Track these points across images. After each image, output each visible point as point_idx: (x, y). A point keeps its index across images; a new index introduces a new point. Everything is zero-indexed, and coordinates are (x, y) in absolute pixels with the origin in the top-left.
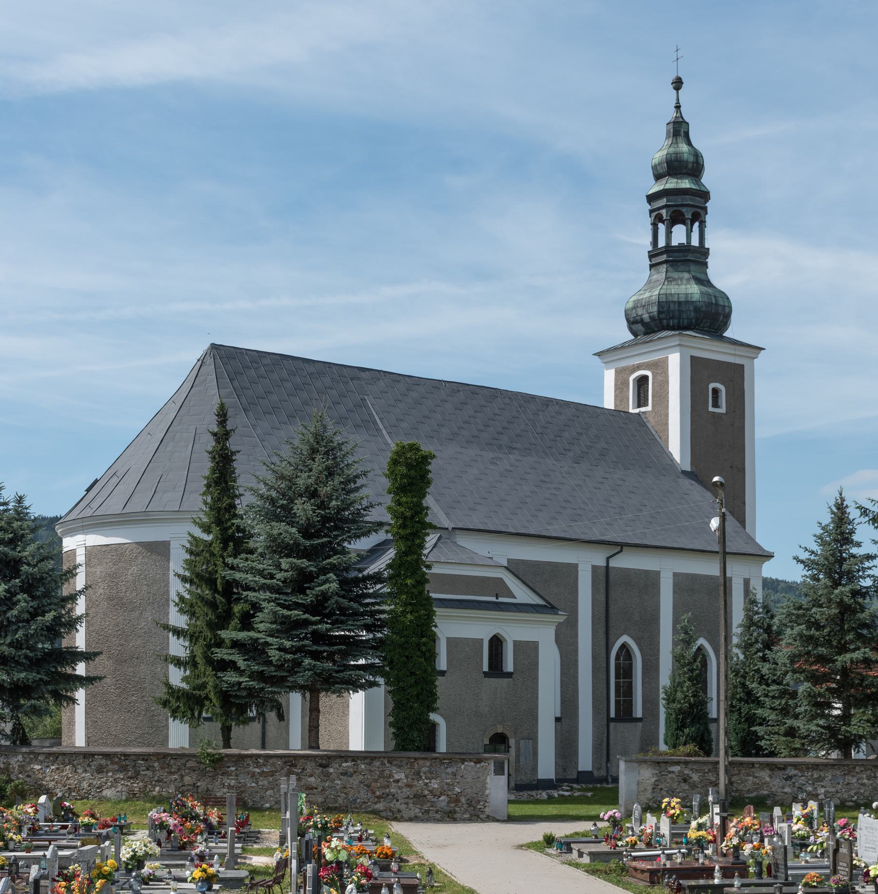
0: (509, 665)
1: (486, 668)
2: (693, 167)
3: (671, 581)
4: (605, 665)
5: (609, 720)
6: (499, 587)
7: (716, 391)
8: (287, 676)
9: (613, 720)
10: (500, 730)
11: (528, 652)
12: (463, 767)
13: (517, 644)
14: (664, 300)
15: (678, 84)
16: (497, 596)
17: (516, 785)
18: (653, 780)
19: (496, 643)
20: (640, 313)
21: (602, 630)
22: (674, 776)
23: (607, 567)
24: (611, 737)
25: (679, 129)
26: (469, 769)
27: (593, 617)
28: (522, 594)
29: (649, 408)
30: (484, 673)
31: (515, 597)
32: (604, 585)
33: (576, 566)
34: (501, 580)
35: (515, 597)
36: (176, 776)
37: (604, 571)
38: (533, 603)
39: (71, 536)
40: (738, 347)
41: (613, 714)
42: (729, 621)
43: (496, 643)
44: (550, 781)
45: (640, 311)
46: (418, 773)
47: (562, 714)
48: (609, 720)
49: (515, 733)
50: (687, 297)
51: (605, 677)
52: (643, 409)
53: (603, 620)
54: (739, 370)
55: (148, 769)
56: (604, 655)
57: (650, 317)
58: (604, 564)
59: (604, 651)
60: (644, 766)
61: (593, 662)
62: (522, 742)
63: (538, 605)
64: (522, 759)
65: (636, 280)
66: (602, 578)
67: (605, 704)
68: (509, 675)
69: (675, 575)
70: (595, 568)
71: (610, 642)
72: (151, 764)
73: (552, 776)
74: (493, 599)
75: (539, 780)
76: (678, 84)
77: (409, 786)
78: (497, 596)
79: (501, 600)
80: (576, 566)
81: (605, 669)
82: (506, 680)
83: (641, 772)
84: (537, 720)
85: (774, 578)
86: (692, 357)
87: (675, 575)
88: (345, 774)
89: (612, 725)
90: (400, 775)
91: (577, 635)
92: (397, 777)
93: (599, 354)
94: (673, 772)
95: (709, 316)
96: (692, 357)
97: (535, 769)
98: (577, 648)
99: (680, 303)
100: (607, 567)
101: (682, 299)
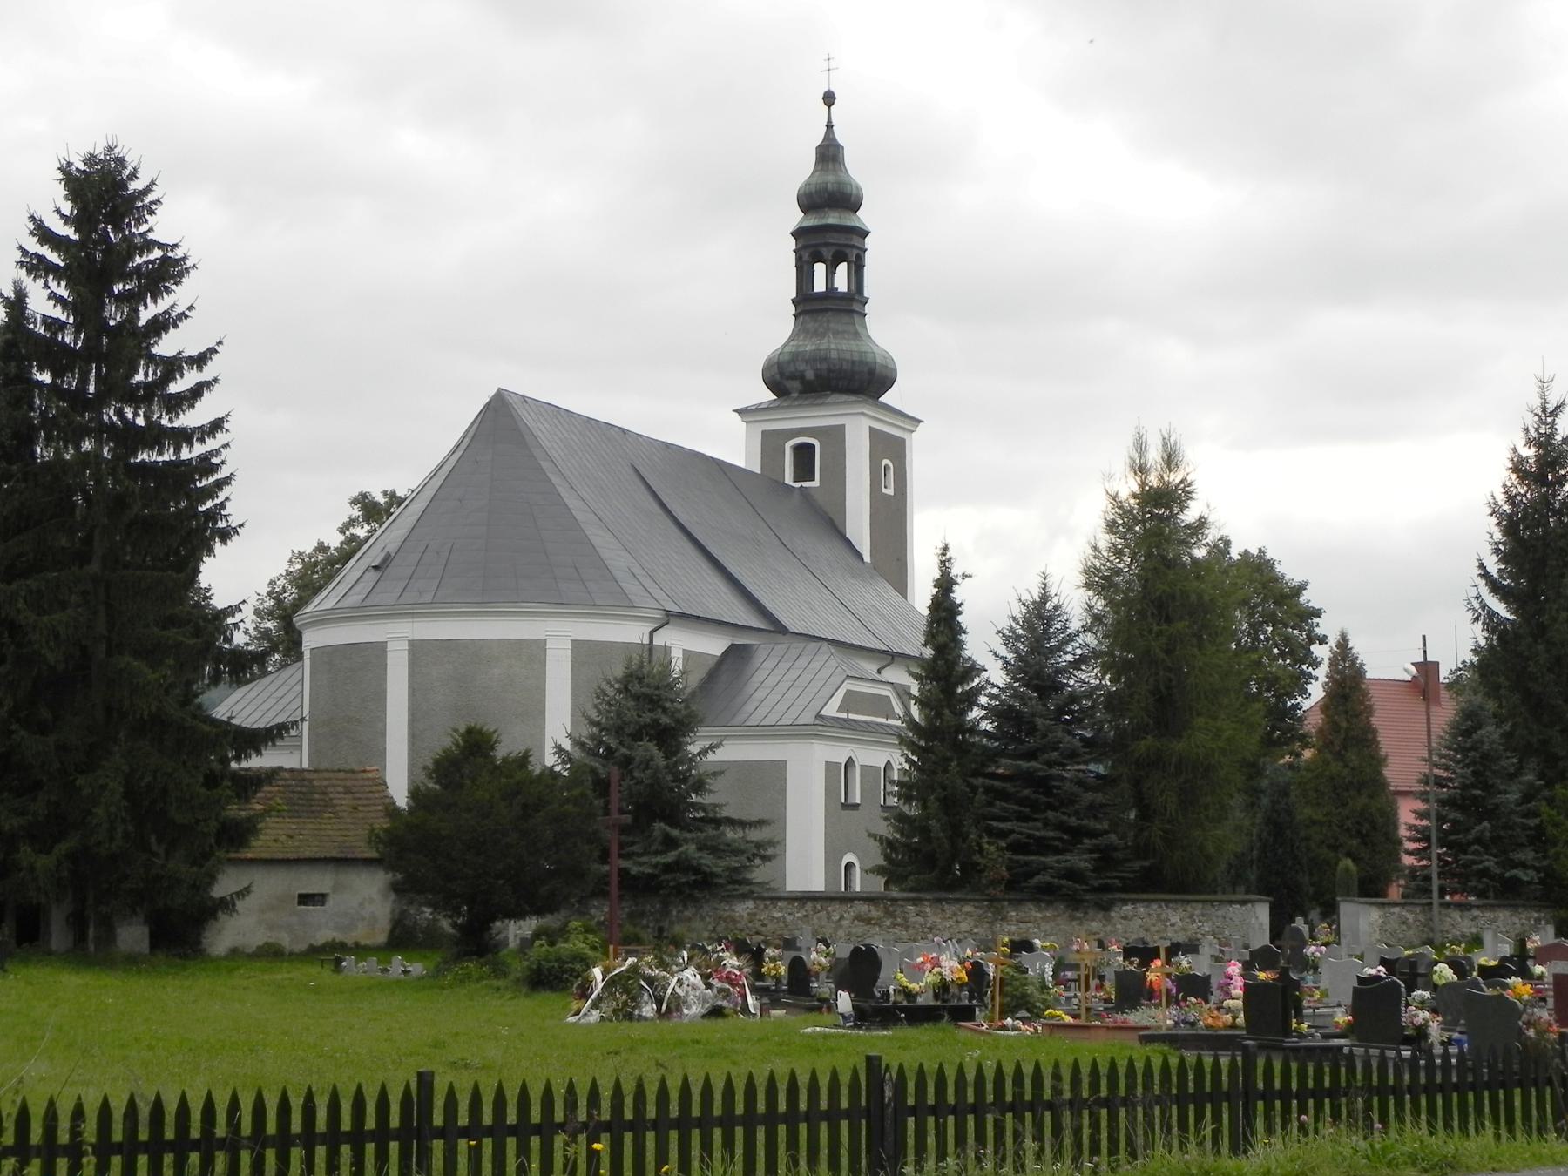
2: (849, 201)
15: (829, 99)
25: (829, 153)
29: (816, 483)
39: (1369, 711)
45: (802, 367)
46: (1191, 916)
54: (901, 444)
58: (646, 641)
65: (774, 327)
69: (577, 646)
73: (817, 884)
76: (829, 99)
77: (1183, 929)
85: (1375, 721)
87: (577, 646)
88: (1125, 918)
90: (1175, 919)
92: (1173, 920)
95: (867, 381)
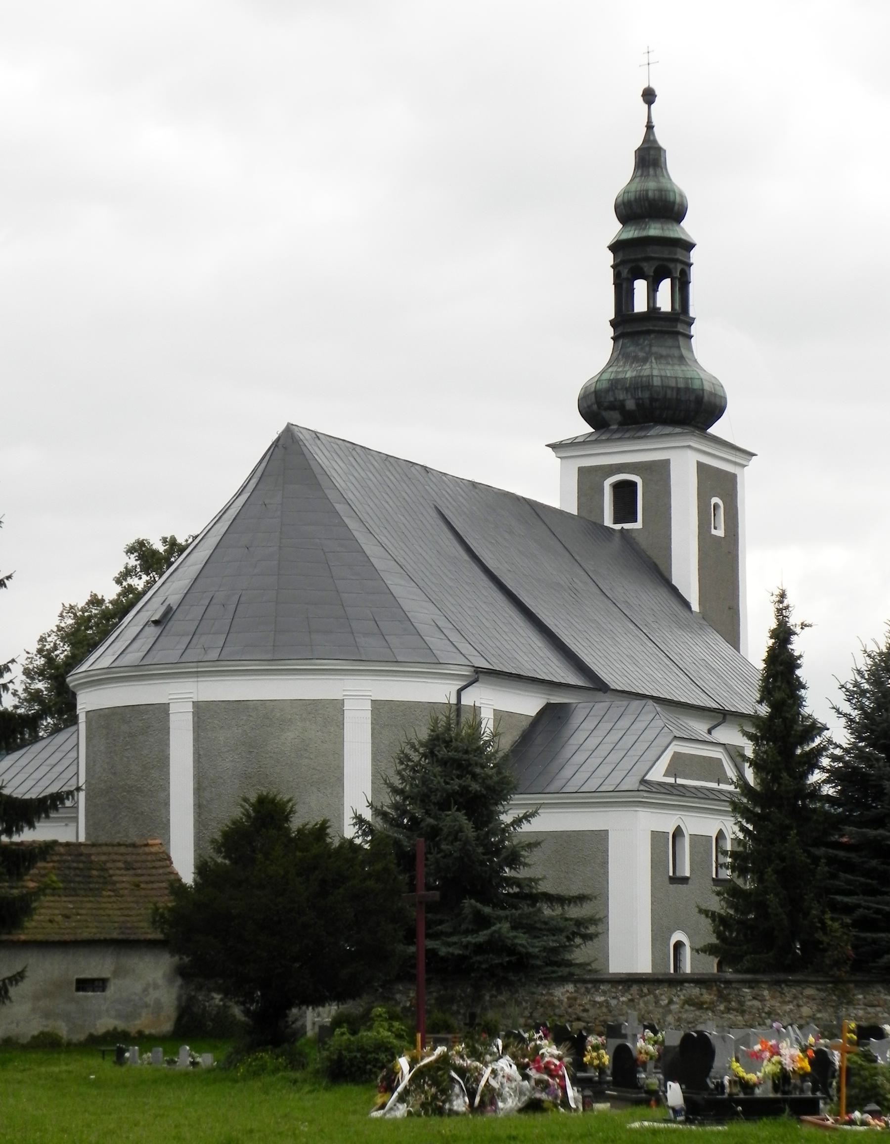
2: (671, 210)
7: (716, 506)
14: (659, 383)
15: (649, 96)
20: (621, 397)
25: (649, 157)
29: (638, 525)
36: (791, 1007)
40: (738, 453)
45: (621, 396)
50: (687, 383)
52: (627, 526)
54: (731, 480)
55: (754, 998)
57: (637, 405)
58: (453, 701)
65: (592, 353)
69: (377, 706)
72: (760, 993)
76: (649, 96)
86: (698, 462)
87: (377, 706)
93: (553, 446)
95: (695, 410)
96: (698, 462)
99: (678, 390)
101: (681, 385)
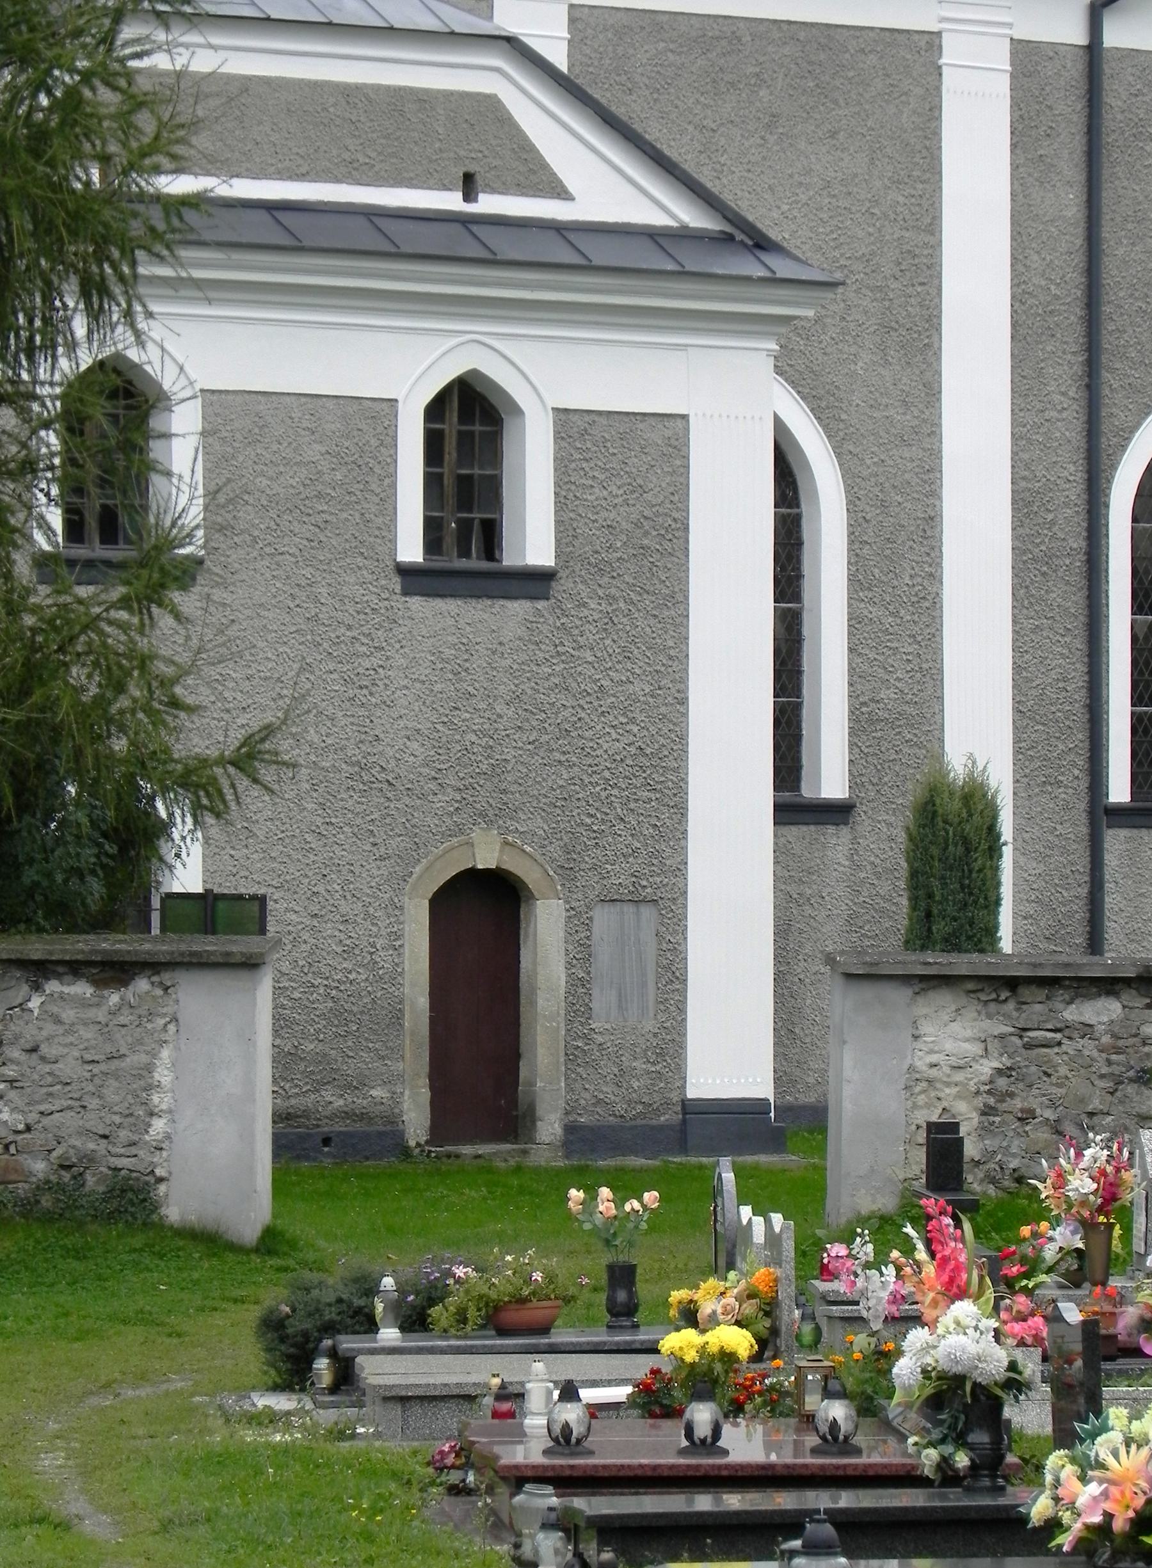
0: (533, 540)
1: (411, 548)
3: (999, 89)
4: (1078, 543)
5: (1103, 815)
6: (483, 147)
8: (101, 668)
9: (1118, 815)
10: (486, 858)
11: (633, 470)
12: (35, 1003)
13: (571, 425)
16: (469, 186)
17: (571, 1129)
18: (986, 1068)
19: (469, 419)
21: (1064, 370)
22: (1088, 1048)
23: (1093, 49)
24: (1112, 900)
26: (69, 1014)
27: (1017, 300)
28: (601, 186)
30: (406, 572)
31: (560, 192)
32: (1078, 143)
33: (931, 42)
34: (489, 109)
35: (560, 192)
37: (1076, 70)
38: (659, 220)
41: (1119, 789)
42: (410, 214)
43: (469, 419)
44: (753, 1108)
47: (855, 782)
48: (1103, 815)
49: (568, 873)
51: (1076, 602)
53: (1075, 314)
56: (1075, 492)
59: (1073, 472)
60: (944, 1000)
61: (1017, 525)
62: (603, 919)
63: (652, 235)
64: (602, 1001)
66: (1069, 109)
67: (1080, 736)
68: (536, 582)
70: (1027, 58)
71: (1106, 441)
74: (451, 201)
75: (694, 1110)
78: (469, 186)
79: (488, 204)
80: (931, 42)
81: (1079, 563)
82: (519, 608)
83: (926, 1028)
84: (681, 810)
89: (1116, 841)
91: (932, 392)
94: (1087, 1030)
97: (669, 1047)
98: (935, 455)
100: (1093, 49)
